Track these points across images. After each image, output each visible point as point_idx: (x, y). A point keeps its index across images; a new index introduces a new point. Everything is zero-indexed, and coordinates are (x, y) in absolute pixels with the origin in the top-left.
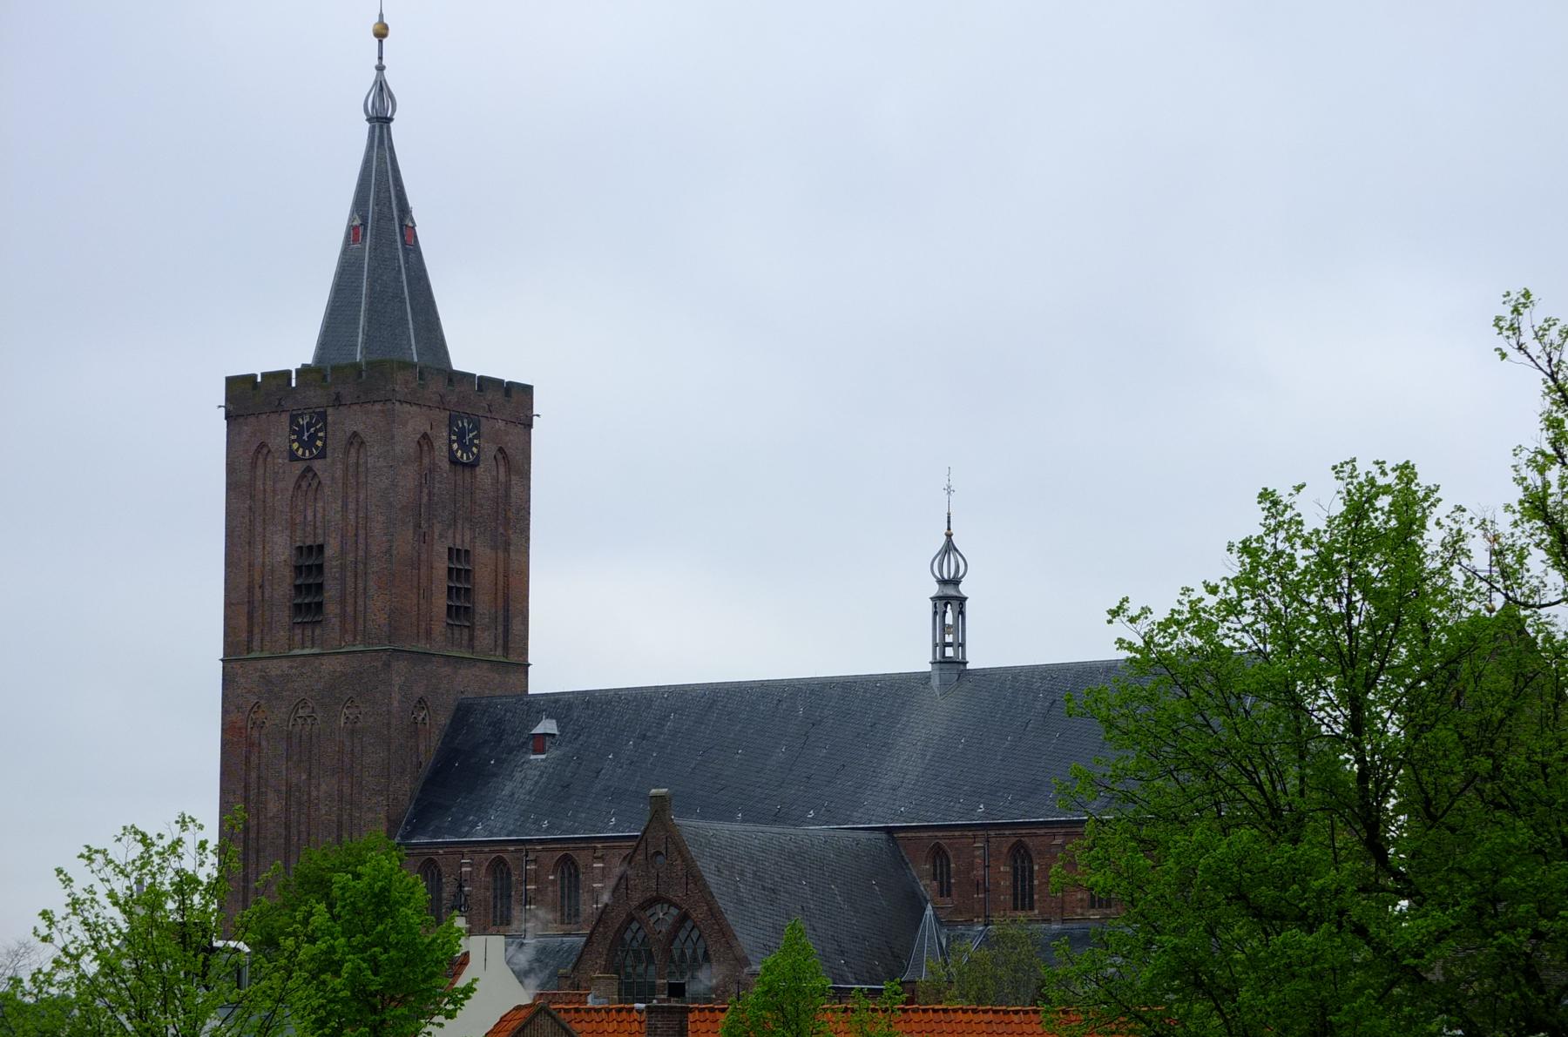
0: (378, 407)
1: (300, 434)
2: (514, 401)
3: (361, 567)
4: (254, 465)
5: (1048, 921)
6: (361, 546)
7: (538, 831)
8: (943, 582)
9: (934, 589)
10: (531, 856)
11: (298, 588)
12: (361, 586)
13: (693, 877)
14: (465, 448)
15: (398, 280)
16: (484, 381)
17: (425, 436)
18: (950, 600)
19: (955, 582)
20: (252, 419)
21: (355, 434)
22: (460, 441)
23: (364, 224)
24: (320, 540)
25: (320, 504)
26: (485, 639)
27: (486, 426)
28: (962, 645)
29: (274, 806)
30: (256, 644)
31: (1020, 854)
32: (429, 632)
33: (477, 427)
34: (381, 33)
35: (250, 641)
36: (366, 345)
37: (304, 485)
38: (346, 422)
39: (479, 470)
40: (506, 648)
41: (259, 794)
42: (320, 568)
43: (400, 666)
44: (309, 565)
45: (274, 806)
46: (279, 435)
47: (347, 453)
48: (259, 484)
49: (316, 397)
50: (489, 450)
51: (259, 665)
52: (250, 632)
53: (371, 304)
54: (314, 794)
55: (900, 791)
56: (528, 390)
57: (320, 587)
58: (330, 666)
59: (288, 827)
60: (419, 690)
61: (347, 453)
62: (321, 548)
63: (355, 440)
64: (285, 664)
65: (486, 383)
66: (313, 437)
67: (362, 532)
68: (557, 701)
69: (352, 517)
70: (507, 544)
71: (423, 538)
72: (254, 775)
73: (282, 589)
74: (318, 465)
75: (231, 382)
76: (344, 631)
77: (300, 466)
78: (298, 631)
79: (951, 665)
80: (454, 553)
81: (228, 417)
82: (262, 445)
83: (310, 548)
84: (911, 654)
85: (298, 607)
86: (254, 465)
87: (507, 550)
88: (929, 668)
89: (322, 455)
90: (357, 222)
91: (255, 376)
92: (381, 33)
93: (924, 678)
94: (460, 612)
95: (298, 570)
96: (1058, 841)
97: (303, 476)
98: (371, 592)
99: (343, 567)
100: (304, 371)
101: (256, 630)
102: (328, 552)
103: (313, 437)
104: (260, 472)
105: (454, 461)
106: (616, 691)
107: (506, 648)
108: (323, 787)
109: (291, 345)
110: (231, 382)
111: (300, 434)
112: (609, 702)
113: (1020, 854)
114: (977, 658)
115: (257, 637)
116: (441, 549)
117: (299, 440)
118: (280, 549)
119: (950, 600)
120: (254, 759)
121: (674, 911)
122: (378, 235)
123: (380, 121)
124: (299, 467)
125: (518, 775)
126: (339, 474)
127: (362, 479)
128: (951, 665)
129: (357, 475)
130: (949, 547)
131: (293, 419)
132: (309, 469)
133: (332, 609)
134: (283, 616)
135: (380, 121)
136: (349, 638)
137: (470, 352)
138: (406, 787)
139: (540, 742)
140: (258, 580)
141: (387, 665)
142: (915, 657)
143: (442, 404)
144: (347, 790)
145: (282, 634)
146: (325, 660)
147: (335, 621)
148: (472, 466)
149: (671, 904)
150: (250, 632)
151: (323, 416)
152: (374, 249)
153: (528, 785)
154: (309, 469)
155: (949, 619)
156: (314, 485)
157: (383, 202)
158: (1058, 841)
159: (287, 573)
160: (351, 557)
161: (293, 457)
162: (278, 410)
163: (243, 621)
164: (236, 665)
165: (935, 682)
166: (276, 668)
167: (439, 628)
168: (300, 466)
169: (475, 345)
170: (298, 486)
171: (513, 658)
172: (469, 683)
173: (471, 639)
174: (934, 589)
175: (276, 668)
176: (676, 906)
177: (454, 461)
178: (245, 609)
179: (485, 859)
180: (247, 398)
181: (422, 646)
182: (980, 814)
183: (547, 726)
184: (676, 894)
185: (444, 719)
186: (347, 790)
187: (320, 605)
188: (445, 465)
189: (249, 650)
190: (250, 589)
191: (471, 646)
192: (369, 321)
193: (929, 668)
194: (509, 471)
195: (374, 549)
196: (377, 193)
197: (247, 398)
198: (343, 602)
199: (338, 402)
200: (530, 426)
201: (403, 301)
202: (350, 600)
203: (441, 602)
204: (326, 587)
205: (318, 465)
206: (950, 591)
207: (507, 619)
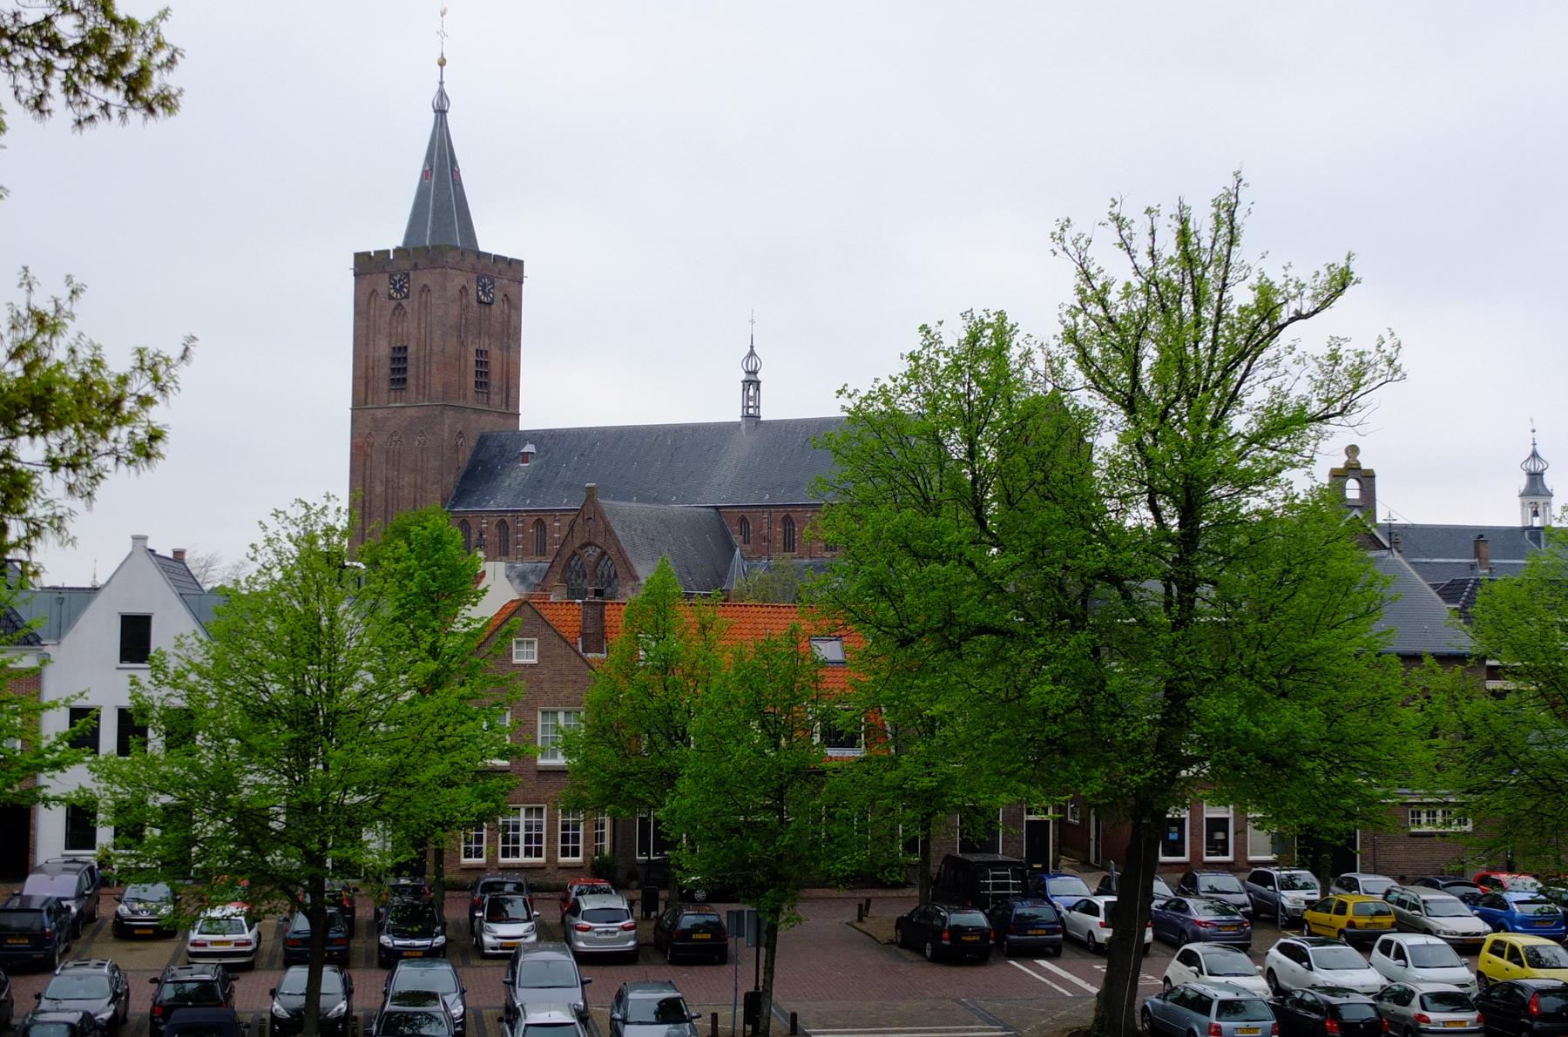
2: (512, 269)
4: (369, 302)
8: (748, 372)
9: (744, 376)
13: (609, 531)
18: (752, 382)
19: (755, 373)
26: (496, 399)
29: (379, 489)
31: (788, 521)
34: (442, 63)
38: (422, 278)
43: (450, 413)
44: (399, 357)
45: (379, 489)
46: (384, 285)
49: (405, 265)
50: (499, 296)
55: (724, 486)
56: (520, 263)
57: (405, 369)
60: (459, 427)
64: (385, 412)
73: (384, 371)
74: (404, 302)
75: (357, 255)
76: (418, 394)
79: (752, 418)
80: (479, 352)
84: (729, 411)
86: (369, 302)
89: (407, 296)
92: (442, 63)
93: (737, 425)
94: (482, 385)
95: (393, 359)
99: (418, 359)
100: (397, 250)
103: (402, 287)
105: (480, 302)
109: (390, 235)
110: (357, 255)
113: (788, 521)
118: (383, 349)
119: (752, 382)
122: (439, 175)
123: (441, 112)
124: (394, 303)
128: (752, 418)
130: (752, 353)
131: (391, 277)
133: (411, 381)
134: (384, 385)
135: (441, 112)
137: (490, 240)
138: (452, 480)
139: (526, 457)
142: (733, 414)
143: (474, 270)
145: (384, 396)
147: (413, 388)
148: (490, 304)
151: (407, 275)
155: (751, 393)
157: (441, 157)
159: (387, 362)
161: (391, 298)
162: (383, 271)
165: (743, 427)
166: (380, 414)
172: (487, 424)
175: (380, 414)
177: (480, 302)
180: (366, 265)
181: (461, 403)
182: (766, 499)
183: (529, 448)
184: (599, 541)
185: (473, 444)
195: (435, 349)
197: (366, 265)
198: (418, 378)
199: (416, 267)
203: (472, 379)
205: (404, 302)
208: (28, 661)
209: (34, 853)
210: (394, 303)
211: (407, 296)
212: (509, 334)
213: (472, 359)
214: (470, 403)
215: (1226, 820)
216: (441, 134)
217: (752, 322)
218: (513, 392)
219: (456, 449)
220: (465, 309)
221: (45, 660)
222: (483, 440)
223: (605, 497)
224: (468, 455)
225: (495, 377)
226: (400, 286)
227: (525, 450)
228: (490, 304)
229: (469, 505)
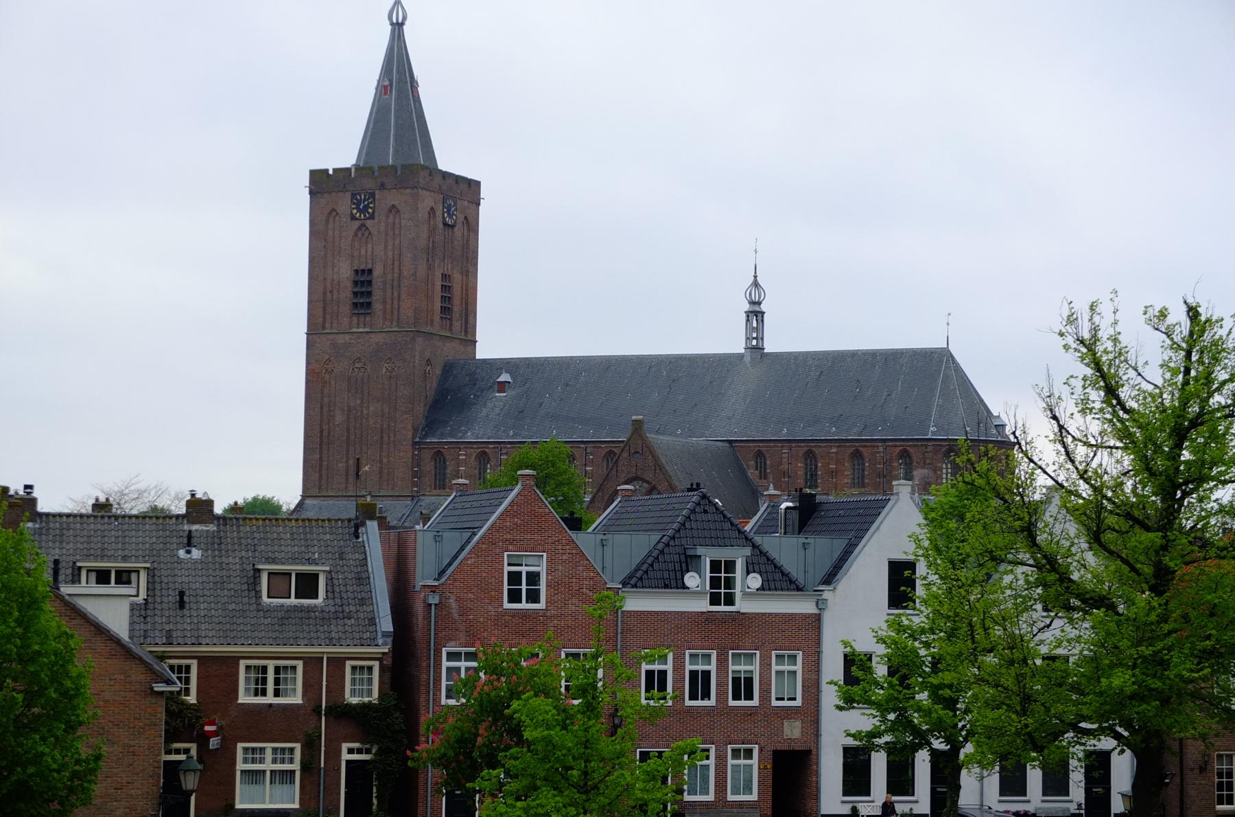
0: (408, 191)
1: (358, 205)
2: (468, 190)
3: (396, 283)
4: (327, 222)
5: (827, 494)
6: (396, 270)
7: (507, 437)
8: (752, 303)
9: (747, 307)
10: (504, 451)
11: (355, 294)
12: (396, 294)
13: (658, 466)
14: (450, 216)
15: (411, 118)
16: (458, 177)
17: (432, 209)
18: (755, 314)
19: (759, 303)
20: (326, 195)
21: (393, 206)
22: (448, 212)
23: (391, 85)
24: (369, 266)
25: (370, 246)
26: (457, 325)
27: (459, 203)
28: (747, 339)
29: (339, 418)
30: (328, 325)
31: (810, 456)
32: (432, 321)
33: (455, 204)
35: (324, 323)
36: (396, 151)
37: (360, 234)
39: (456, 229)
40: (466, 332)
41: (330, 411)
42: (370, 283)
43: (420, 340)
44: (363, 281)
45: (339, 418)
46: (345, 205)
47: (387, 217)
48: (330, 233)
49: (369, 184)
51: (330, 337)
52: (324, 318)
53: (396, 131)
54: (365, 412)
55: (733, 420)
56: (478, 184)
57: (369, 294)
58: (375, 338)
59: (348, 431)
60: (428, 355)
61: (387, 217)
62: (370, 271)
63: (393, 209)
64: (347, 337)
65: (458, 179)
66: (366, 207)
67: (396, 263)
68: (796, 358)
69: (390, 254)
70: (467, 272)
71: (430, 267)
72: (326, 400)
73: (346, 294)
74: (369, 223)
75: (313, 173)
76: (385, 319)
77: (357, 223)
78: (355, 318)
79: (756, 349)
80: (445, 277)
81: (311, 193)
82: (334, 210)
83: (363, 271)
84: (733, 342)
85: (355, 305)
86: (327, 222)
87: (467, 275)
88: (743, 351)
89: (372, 217)
90: (387, 83)
91: (327, 170)
93: (740, 357)
94: (446, 310)
95: (356, 283)
96: (834, 450)
97: (359, 228)
98: (403, 297)
99: (384, 283)
100: (357, 167)
101: (328, 317)
102: (376, 273)
103: (366, 207)
104: (331, 226)
105: (445, 224)
106: (546, 359)
107: (466, 332)
108: (371, 409)
109: (344, 153)
110: (313, 173)
111: (358, 205)
112: (542, 365)
114: (769, 347)
115: (328, 320)
116: (438, 274)
117: (358, 208)
118: (344, 271)
119: (755, 314)
120: (326, 391)
121: (645, 485)
122: (399, 91)
123: (398, 28)
124: (357, 224)
125: (490, 405)
126: (382, 228)
127: (397, 232)
128: (756, 349)
129: (393, 229)
130: (756, 284)
131: (353, 196)
132: (363, 225)
133: (377, 306)
134: (346, 309)
135: (398, 28)
136: (387, 323)
137: (450, 159)
138: (420, 409)
139: (502, 386)
140: (329, 287)
141: (413, 339)
143: (440, 191)
144: (386, 410)
146: (372, 335)
147: (380, 313)
148: (453, 226)
149: (644, 480)
150: (324, 318)
151: (373, 195)
152: (397, 99)
153: (497, 410)
154: (363, 225)
155: (755, 325)
156: (366, 234)
158: (834, 450)
159: (349, 284)
160: (390, 276)
161: (353, 218)
162: (344, 190)
163: (320, 312)
164: (316, 337)
165: (747, 359)
166: (341, 339)
167: (437, 318)
168: (357, 223)
169: (451, 158)
170: (356, 235)
171: (469, 338)
172: (449, 351)
173: (451, 325)
174: (747, 307)
175: (341, 339)
176: (648, 482)
177: (445, 224)
178: (321, 304)
179: (474, 452)
180: (320, 183)
181: (428, 329)
182: (784, 434)
183: (505, 377)
184: (649, 476)
185: (438, 371)
186: (386, 410)
187: (369, 304)
188: (441, 226)
189: (324, 328)
190: (325, 294)
191: (451, 330)
192: (396, 140)
193: (743, 351)
194: (469, 230)
195: (405, 273)
196: (398, 66)
197: (320, 183)
198: (384, 302)
199: (382, 187)
200: (479, 204)
201: (414, 130)
202: (389, 301)
203: (438, 305)
204: (374, 293)
205: (369, 223)
206: (756, 308)
207: (467, 315)
208: (802, 606)
209: (817, 798)
210: (357, 224)
211: (372, 217)
212: (467, 257)
213: (438, 283)
214: (436, 329)
215: (294, 771)
216: (400, 48)
217: (756, 251)
218: (471, 318)
219: (425, 376)
220: (432, 230)
221: (821, 604)
222: (448, 368)
223: (650, 432)
224: (435, 385)
225: (456, 306)
226: (364, 205)
227: (501, 379)
228: (453, 226)
229: (442, 435)
